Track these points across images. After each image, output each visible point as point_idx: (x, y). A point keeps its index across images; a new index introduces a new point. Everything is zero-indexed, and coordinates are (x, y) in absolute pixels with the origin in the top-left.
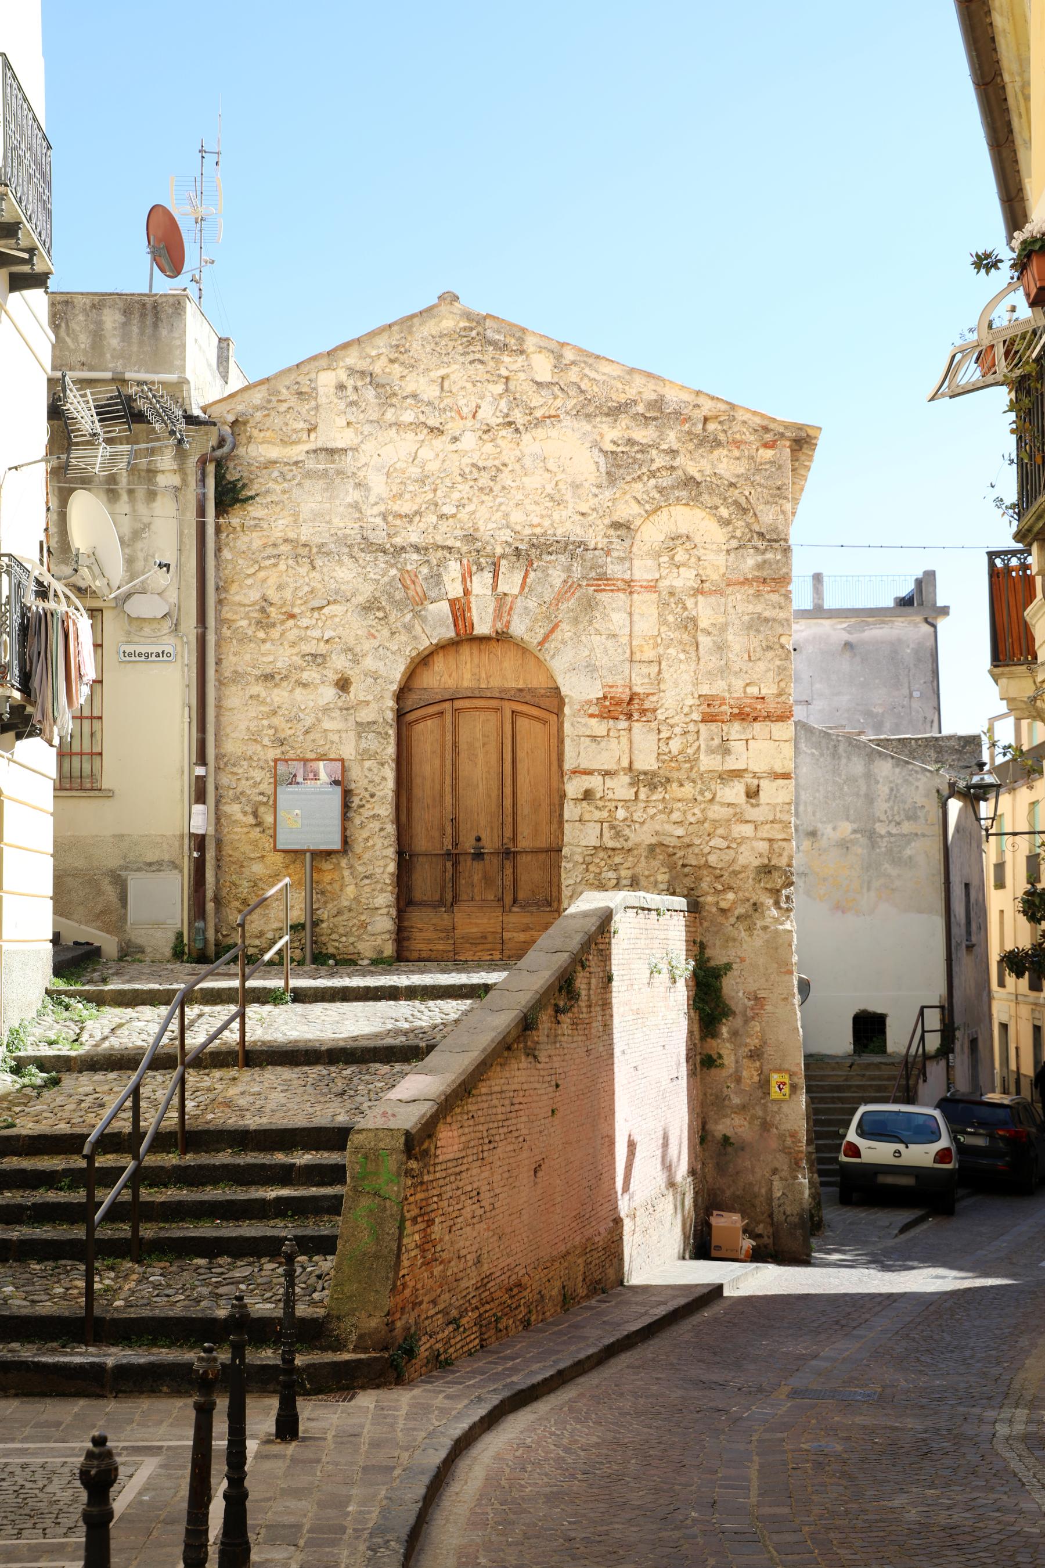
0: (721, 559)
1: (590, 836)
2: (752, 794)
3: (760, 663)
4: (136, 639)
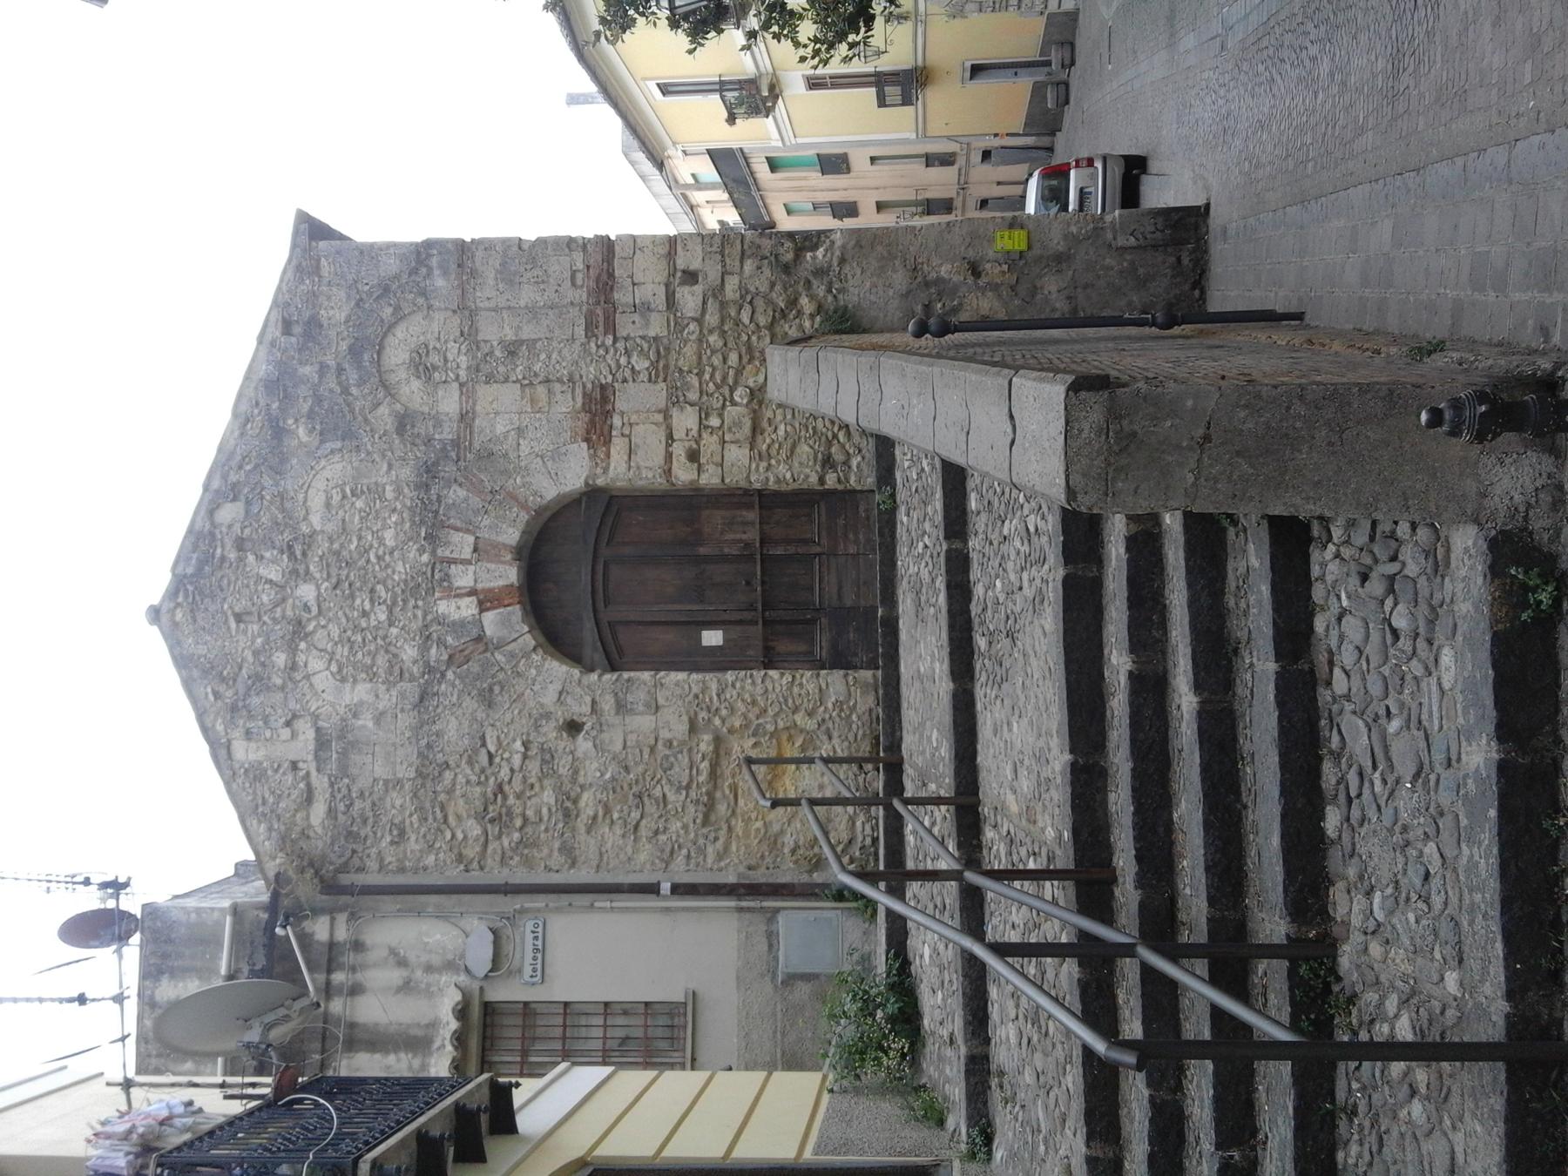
0: (439, 316)
1: (737, 455)
2: (691, 277)
3: (550, 271)
4: (516, 963)
